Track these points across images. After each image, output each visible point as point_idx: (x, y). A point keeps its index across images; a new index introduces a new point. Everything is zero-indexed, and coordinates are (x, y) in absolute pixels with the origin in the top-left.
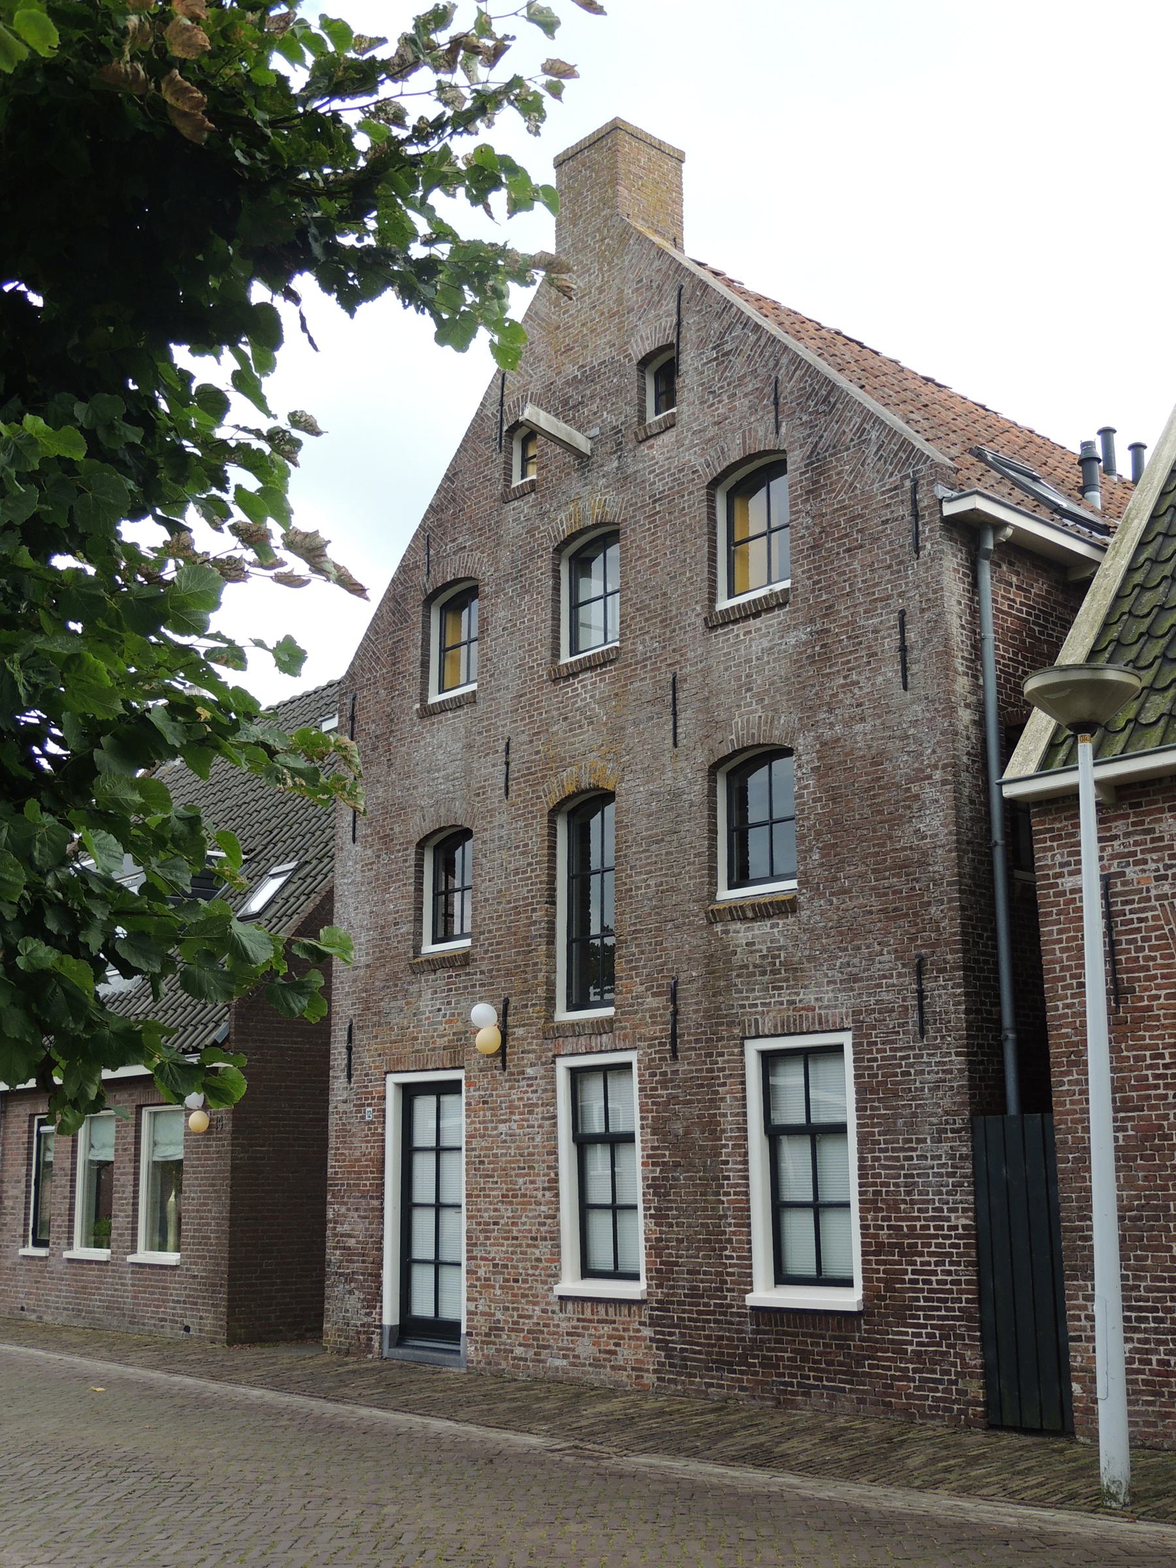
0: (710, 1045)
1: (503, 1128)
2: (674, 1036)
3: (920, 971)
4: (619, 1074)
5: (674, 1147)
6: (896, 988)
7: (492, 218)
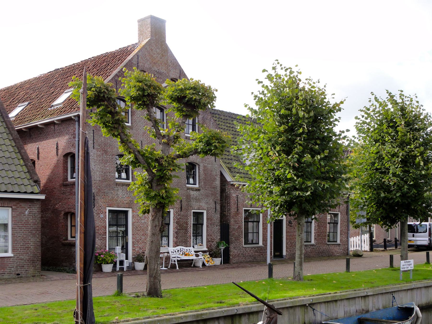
0: (187, 210)
1: (143, 221)
2: (181, 207)
3: (215, 203)
4: (282, 264)
5: (180, 226)
6: (212, 205)
7: (221, 172)
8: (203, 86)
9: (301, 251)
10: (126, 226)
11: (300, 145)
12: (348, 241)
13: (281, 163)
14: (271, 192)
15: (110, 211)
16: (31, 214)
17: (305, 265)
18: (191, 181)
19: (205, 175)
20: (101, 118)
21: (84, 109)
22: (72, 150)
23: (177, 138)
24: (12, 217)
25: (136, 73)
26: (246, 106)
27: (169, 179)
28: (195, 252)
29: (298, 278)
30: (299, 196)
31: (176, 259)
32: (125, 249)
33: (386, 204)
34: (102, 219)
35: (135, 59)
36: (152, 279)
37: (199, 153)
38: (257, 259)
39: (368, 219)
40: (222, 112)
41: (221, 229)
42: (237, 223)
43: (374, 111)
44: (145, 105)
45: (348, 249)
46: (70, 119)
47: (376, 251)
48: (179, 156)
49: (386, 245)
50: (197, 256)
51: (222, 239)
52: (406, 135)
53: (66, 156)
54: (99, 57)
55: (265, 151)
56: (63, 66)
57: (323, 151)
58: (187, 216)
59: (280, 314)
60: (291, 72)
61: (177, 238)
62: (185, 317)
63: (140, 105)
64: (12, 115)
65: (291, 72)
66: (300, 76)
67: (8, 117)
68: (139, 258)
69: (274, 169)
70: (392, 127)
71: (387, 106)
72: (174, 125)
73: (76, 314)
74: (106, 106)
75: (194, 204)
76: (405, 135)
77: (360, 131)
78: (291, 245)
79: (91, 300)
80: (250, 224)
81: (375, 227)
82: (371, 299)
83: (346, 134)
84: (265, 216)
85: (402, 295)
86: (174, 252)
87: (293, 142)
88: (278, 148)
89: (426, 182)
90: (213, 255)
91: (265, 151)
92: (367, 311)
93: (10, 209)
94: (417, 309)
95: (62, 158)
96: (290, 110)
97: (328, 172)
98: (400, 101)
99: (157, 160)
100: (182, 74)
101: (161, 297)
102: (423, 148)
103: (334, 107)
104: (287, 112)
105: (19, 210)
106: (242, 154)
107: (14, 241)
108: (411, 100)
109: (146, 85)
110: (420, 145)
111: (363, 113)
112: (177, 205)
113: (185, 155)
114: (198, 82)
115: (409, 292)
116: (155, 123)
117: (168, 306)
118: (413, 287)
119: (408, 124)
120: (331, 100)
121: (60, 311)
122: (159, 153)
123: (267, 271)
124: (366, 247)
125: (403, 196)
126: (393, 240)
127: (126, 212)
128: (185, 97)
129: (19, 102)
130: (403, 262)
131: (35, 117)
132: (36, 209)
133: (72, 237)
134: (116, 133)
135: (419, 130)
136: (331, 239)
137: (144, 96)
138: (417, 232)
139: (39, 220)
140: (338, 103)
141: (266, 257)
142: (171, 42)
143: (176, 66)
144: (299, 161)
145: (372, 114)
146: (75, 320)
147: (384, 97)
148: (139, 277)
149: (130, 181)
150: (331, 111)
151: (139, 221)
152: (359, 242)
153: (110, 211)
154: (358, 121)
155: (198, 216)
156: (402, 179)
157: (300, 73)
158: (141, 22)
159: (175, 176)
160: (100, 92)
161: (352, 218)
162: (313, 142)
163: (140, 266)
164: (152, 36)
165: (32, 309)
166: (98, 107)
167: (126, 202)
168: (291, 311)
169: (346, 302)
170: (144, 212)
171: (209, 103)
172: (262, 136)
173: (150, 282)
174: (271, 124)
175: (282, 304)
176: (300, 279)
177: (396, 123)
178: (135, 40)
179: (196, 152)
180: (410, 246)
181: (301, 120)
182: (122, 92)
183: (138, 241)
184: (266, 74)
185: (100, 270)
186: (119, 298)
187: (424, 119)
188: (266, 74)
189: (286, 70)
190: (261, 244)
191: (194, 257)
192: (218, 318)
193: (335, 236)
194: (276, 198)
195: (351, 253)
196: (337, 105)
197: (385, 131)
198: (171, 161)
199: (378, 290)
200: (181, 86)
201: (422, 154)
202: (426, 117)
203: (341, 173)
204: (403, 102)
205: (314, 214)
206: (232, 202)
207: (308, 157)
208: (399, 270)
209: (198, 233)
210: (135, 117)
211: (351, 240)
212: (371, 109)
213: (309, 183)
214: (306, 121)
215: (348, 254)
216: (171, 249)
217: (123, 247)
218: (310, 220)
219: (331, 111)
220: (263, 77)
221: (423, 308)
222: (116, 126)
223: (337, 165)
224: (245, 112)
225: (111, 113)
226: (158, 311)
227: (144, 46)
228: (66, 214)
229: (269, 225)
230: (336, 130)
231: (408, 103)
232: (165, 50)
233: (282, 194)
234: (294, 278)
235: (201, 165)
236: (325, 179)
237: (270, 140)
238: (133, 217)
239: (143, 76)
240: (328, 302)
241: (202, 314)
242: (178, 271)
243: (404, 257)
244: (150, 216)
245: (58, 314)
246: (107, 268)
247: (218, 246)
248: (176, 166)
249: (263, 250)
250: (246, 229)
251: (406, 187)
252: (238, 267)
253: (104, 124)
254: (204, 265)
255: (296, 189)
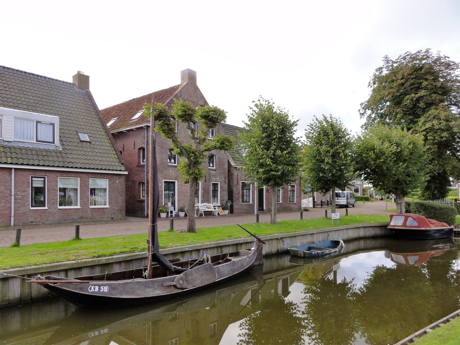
0: (209, 182)
6: (223, 179)
8: (219, 110)
9: (275, 207)
10: (174, 190)
11: (274, 145)
12: (300, 202)
13: (263, 155)
14: (258, 172)
15: (165, 182)
16: (120, 183)
17: (277, 215)
18: (211, 165)
20: (161, 127)
21: (152, 122)
22: (143, 146)
23: (204, 140)
24: (109, 184)
25: (181, 102)
26: (243, 122)
27: (200, 163)
28: (214, 206)
29: (273, 222)
30: (274, 175)
31: (203, 211)
32: (173, 204)
33: (323, 180)
34: (162, 186)
35: (179, 94)
36: (190, 222)
37: (217, 148)
38: (249, 211)
39: (312, 189)
40: (93, 99)
41: (228, 193)
42: (238, 189)
43: (315, 126)
44: (186, 120)
45: (301, 206)
46: (142, 128)
47: (317, 207)
48: (206, 150)
49: (322, 204)
50: (215, 209)
51: (228, 199)
52: (334, 140)
53: (140, 149)
54: (158, 92)
55: (254, 148)
56: (138, 97)
57: (287, 149)
58: (209, 185)
59: (264, 243)
60: (269, 103)
61: (203, 198)
62: (210, 244)
63: (184, 120)
64: (109, 124)
65: (269, 103)
66: (273, 105)
67: (106, 126)
68: (181, 210)
69: (259, 159)
70: (326, 135)
71: (323, 123)
72: (202, 132)
73: (148, 241)
74: (164, 120)
75: (213, 178)
76: (334, 140)
77: (308, 137)
78: (269, 203)
79: (157, 233)
80: (245, 191)
81: (315, 194)
82: (315, 235)
83: (300, 139)
84: (253, 186)
85: (333, 233)
86: (202, 206)
87: (270, 143)
88: (262, 146)
89: (345, 168)
90: (224, 208)
91: (254, 148)
92: (313, 243)
93: (108, 180)
94: (342, 242)
95: (137, 150)
96: (269, 125)
97: (290, 161)
98: (331, 120)
99: (193, 152)
100: (206, 103)
101: (196, 232)
103: (293, 123)
104: (267, 126)
105: (113, 180)
106: (241, 149)
107: (110, 199)
108: (337, 120)
109: (187, 109)
110: (342, 146)
111: (309, 127)
112: (204, 179)
113: (208, 150)
114: (216, 107)
115: (337, 232)
116: (193, 131)
117: (200, 238)
118: (339, 229)
119: (335, 134)
120: (292, 119)
121: (138, 240)
122: (194, 148)
123: (256, 218)
124: (311, 205)
125: (333, 175)
126: (326, 201)
127: (174, 183)
128: (209, 116)
129: (112, 118)
130: (333, 214)
131: (121, 126)
132: (123, 180)
133: (143, 197)
134: (170, 136)
135: (341, 138)
136: (291, 200)
137: (186, 115)
138: (340, 197)
139: (124, 187)
140: (296, 121)
141: (254, 210)
142: (200, 84)
143: (203, 98)
144: (274, 154)
145: (314, 128)
146: (148, 245)
147: (321, 118)
148: (182, 221)
149: (176, 164)
150: (292, 125)
151: (181, 188)
152: (307, 202)
153: (165, 182)
154: (306, 132)
155: (215, 185)
156: (332, 166)
157: (274, 103)
158: (183, 73)
159: (203, 162)
160: (161, 112)
161: (303, 188)
162: (282, 143)
163: (182, 214)
164: (188, 80)
165: (122, 238)
166: (160, 121)
168: (270, 242)
169: (301, 237)
170: (186, 183)
171: (223, 119)
172: (252, 139)
173: (189, 223)
174: (258, 132)
175: (265, 238)
176: (275, 223)
177: (328, 133)
178: (179, 83)
179: (215, 148)
180: (337, 205)
181: (273, 129)
182: (173, 112)
183: (181, 200)
184: (254, 103)
185: (159, 216)
186: (171, 233)
187: (344, 131)
188: (254, 103)
189: (266, 101)
190: (251, 202)
191: (213, 210)
192: (229, 246)
193: (293, 199)
194: (261, 176)
195: (302, 209)
196: (295, 122)
197: (322, 138)
198: (201, 153)
199: (319, 230)
200: (207, 110)
201: (343, 151)
202: (345, 130)
203: (297, 162)
204: (332, 121)
205: (282, 185)
206: (235, 178)
207: (279, 152)
208: (331, 219)
209: (215, 196)
210: (179, 127)
211: (303, 201)
212: (314, 125)
213: (280, 167)
214: (278, 131)
215: (300, 209)
216: (200, 204)
217: (172, 203)
218: (279, 189)
219: (292, 125)
220: (252, 105)
221: (345, 241)
222: (170, 132)
223: (295, 157)
224: (242, 125)
225: (167, 124)
226: (194, 240)
227: (184, 86)
228: (140, 183)
229: (256, 191)
230: (295, 136)
231: (335, 122)
232: (197, 89)
233: (264, 173)
234: (271, 223)
235: (217, 156)
236: (288, 165)
237: (257, 142)
238: (178, 185)
239: (187, 103)
240: (291, 237)
241: (220, 243)
242: (204, 218)
243: (333, 212)
244: (189, 185)
245: (137, 241)
246: (163, 215)
247: (227, 203)
248: (204, 156)
249: (252, 206)
250: (243, 193)
251: (335, 170)
252: (238, 216)
253: (163, 130)
254: (218, 214)
255: (272, 171)
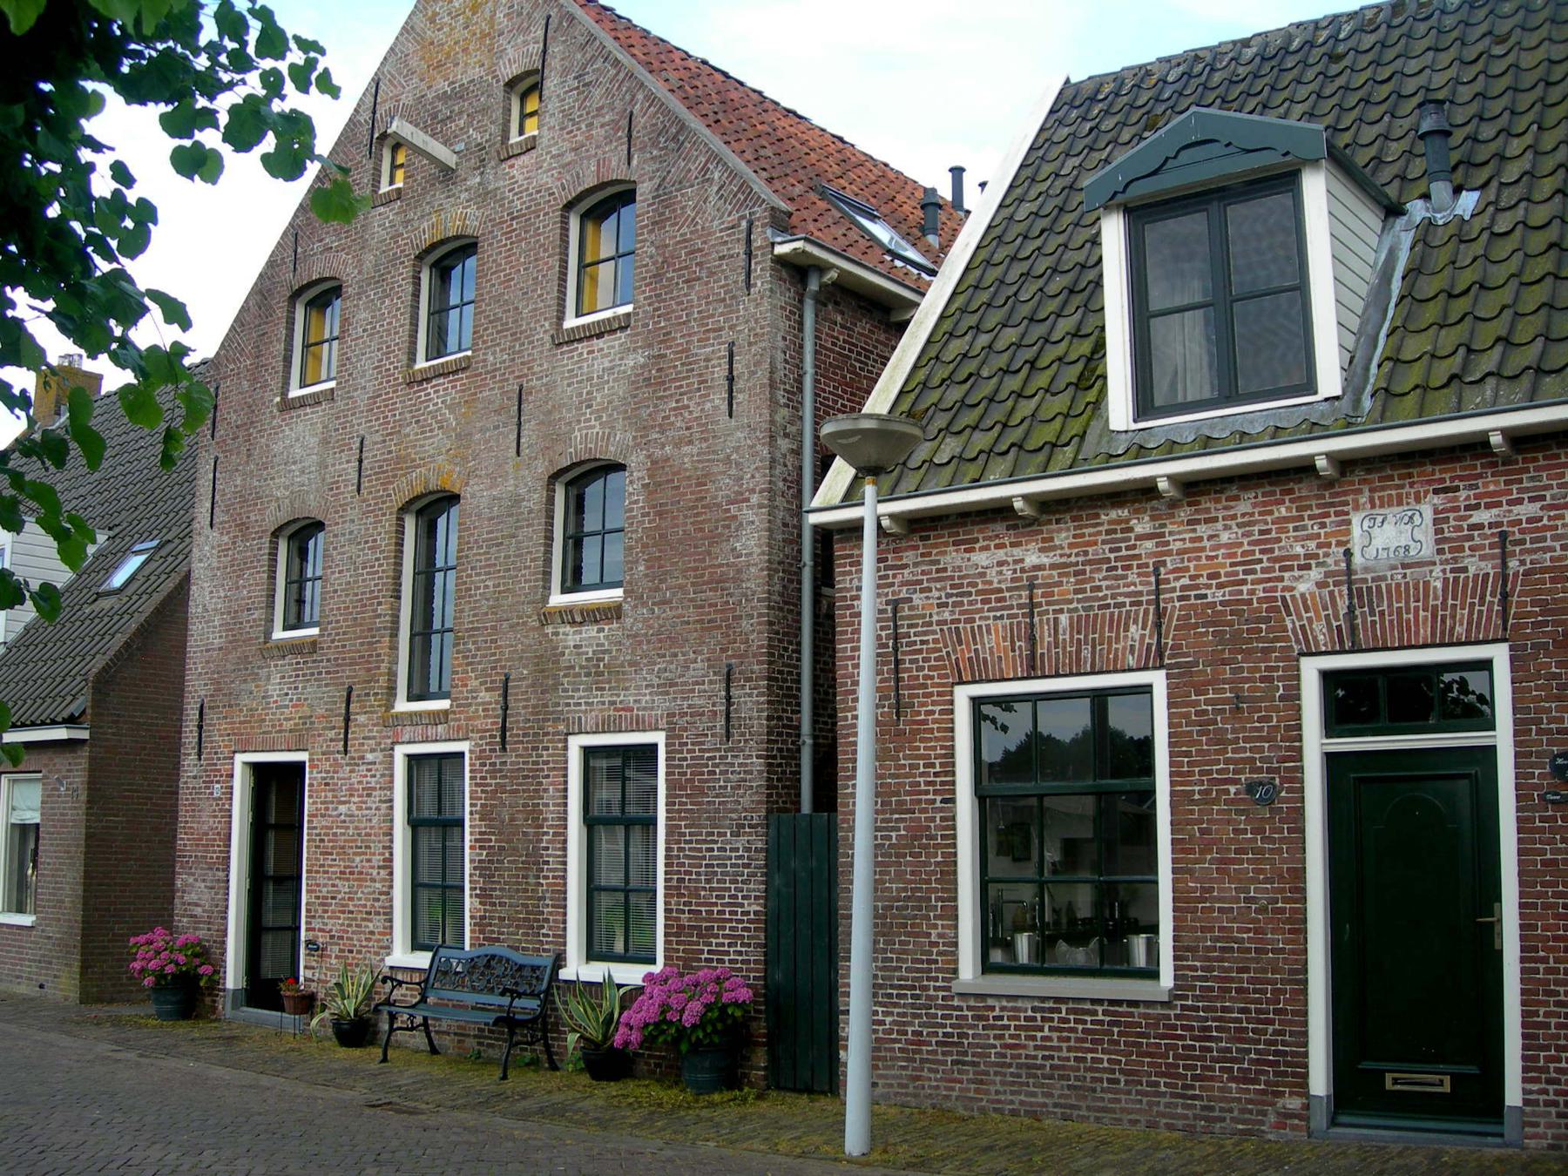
0: (536, 740)
1: (343, 809)
6: (707, 695)
19: (660, 514)
102: (208, 64)
167: (288, 725)
